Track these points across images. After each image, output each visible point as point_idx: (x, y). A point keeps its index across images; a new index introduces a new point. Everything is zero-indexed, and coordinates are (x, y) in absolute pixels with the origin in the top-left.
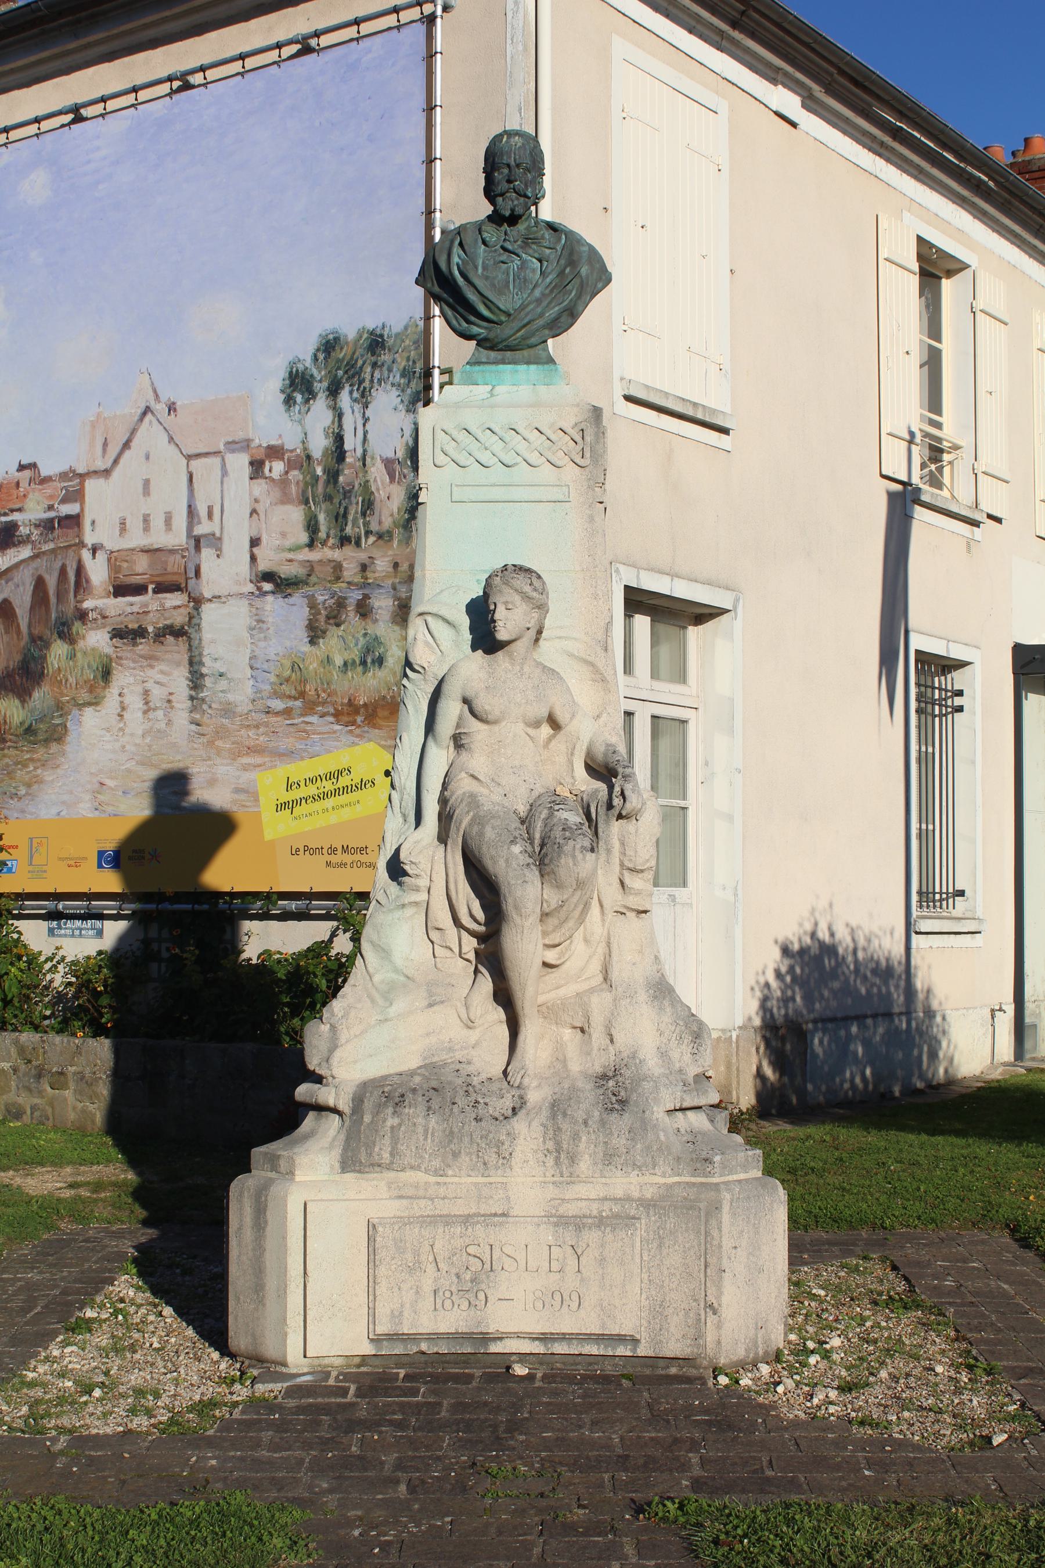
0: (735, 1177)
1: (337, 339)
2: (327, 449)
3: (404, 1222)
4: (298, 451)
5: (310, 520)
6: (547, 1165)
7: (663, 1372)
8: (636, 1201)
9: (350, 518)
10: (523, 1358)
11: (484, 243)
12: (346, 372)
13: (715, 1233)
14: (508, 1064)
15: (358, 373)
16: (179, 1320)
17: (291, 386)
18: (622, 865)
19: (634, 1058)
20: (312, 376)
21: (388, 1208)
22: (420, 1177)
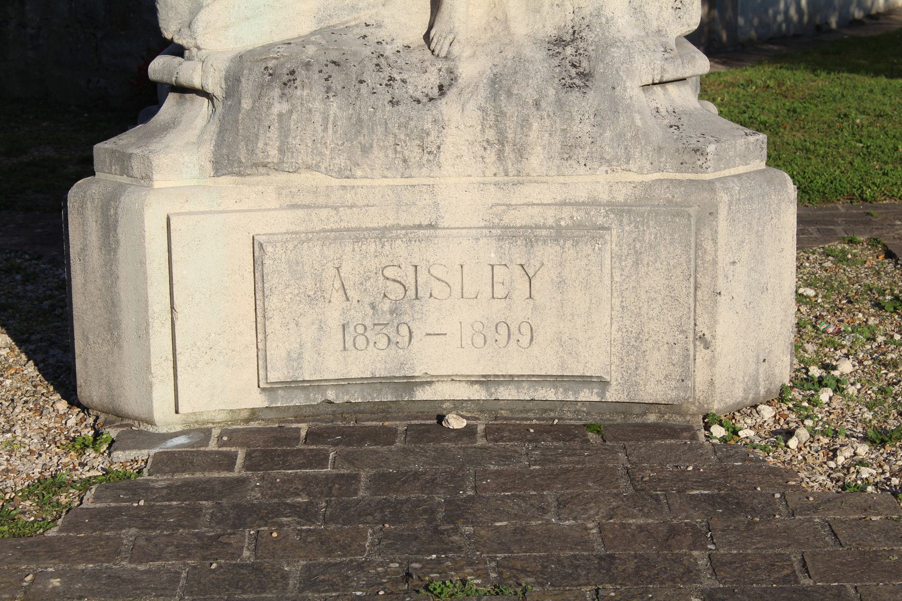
0: (733, 171)
3: (300, 238)
6: (487, 160)
7: (639, 420)
8: (604, 206)
10: (458, 405)
13: (708, 245)
14: (431, 27)
16: (17, 350)
19: (598, 15)
21: (278, 222)
22: (319, 179)
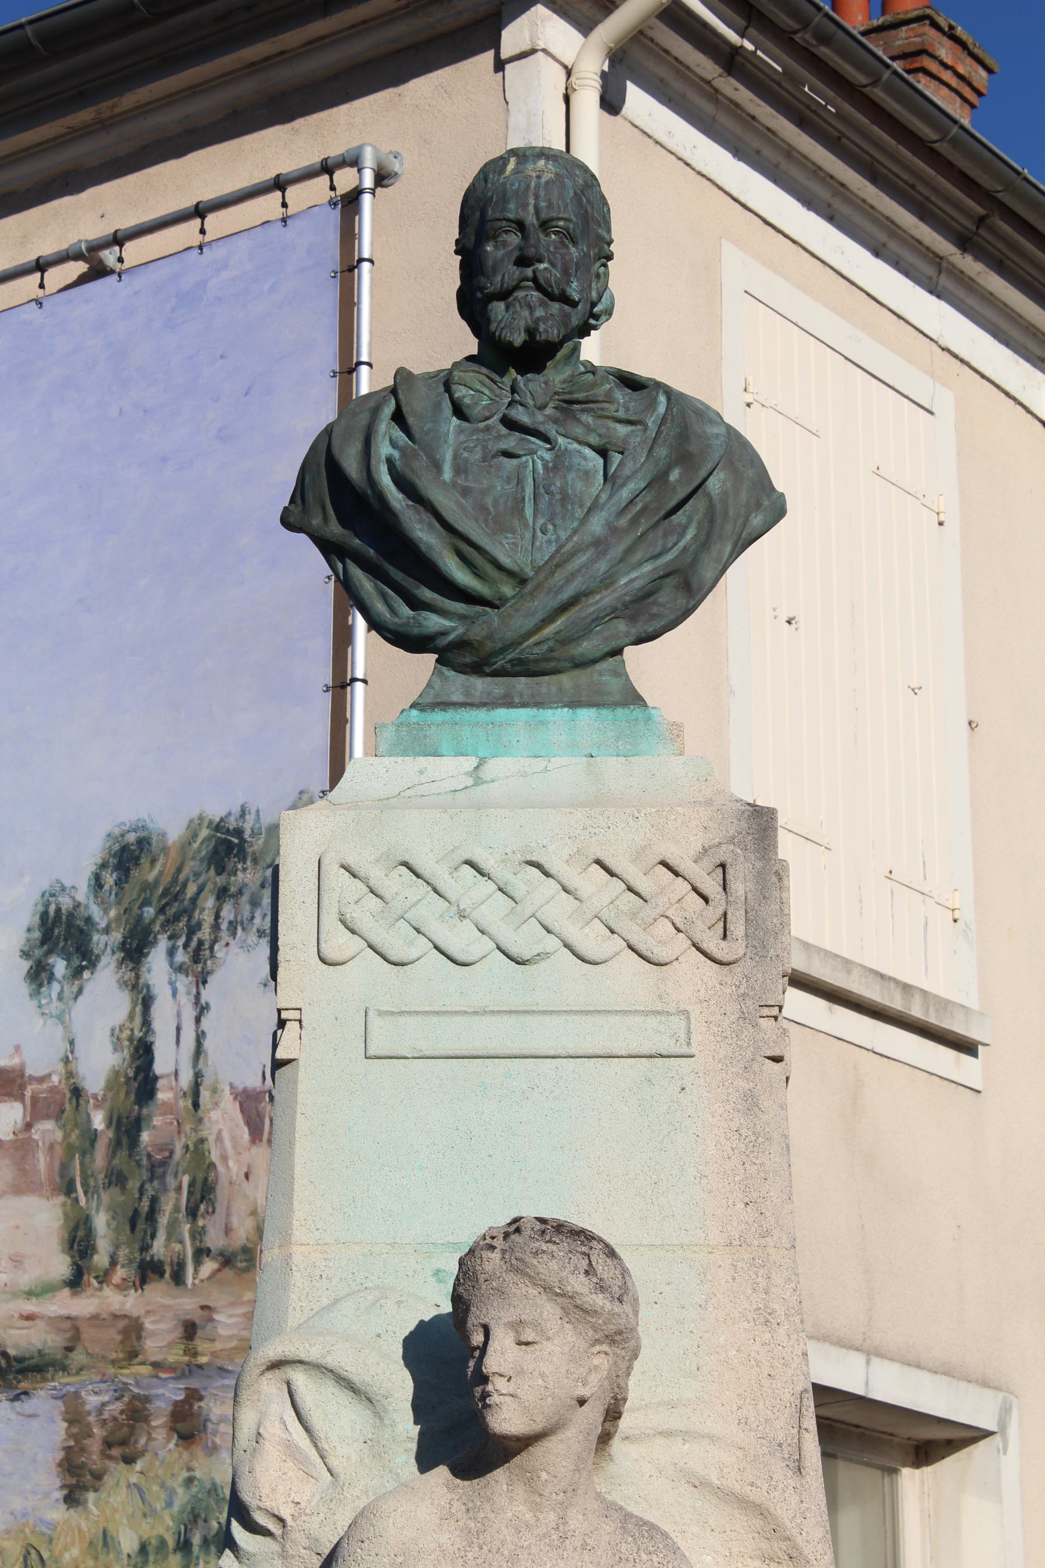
1: (143, 843)
2: (116, 1073)
4: (55, 1079)
5: (76, 1228)
9: (163, 1220)
11: (459, 411)
12: (161, 910)
15: (188, 912)
17: (43, 942)
20: (89, 920)
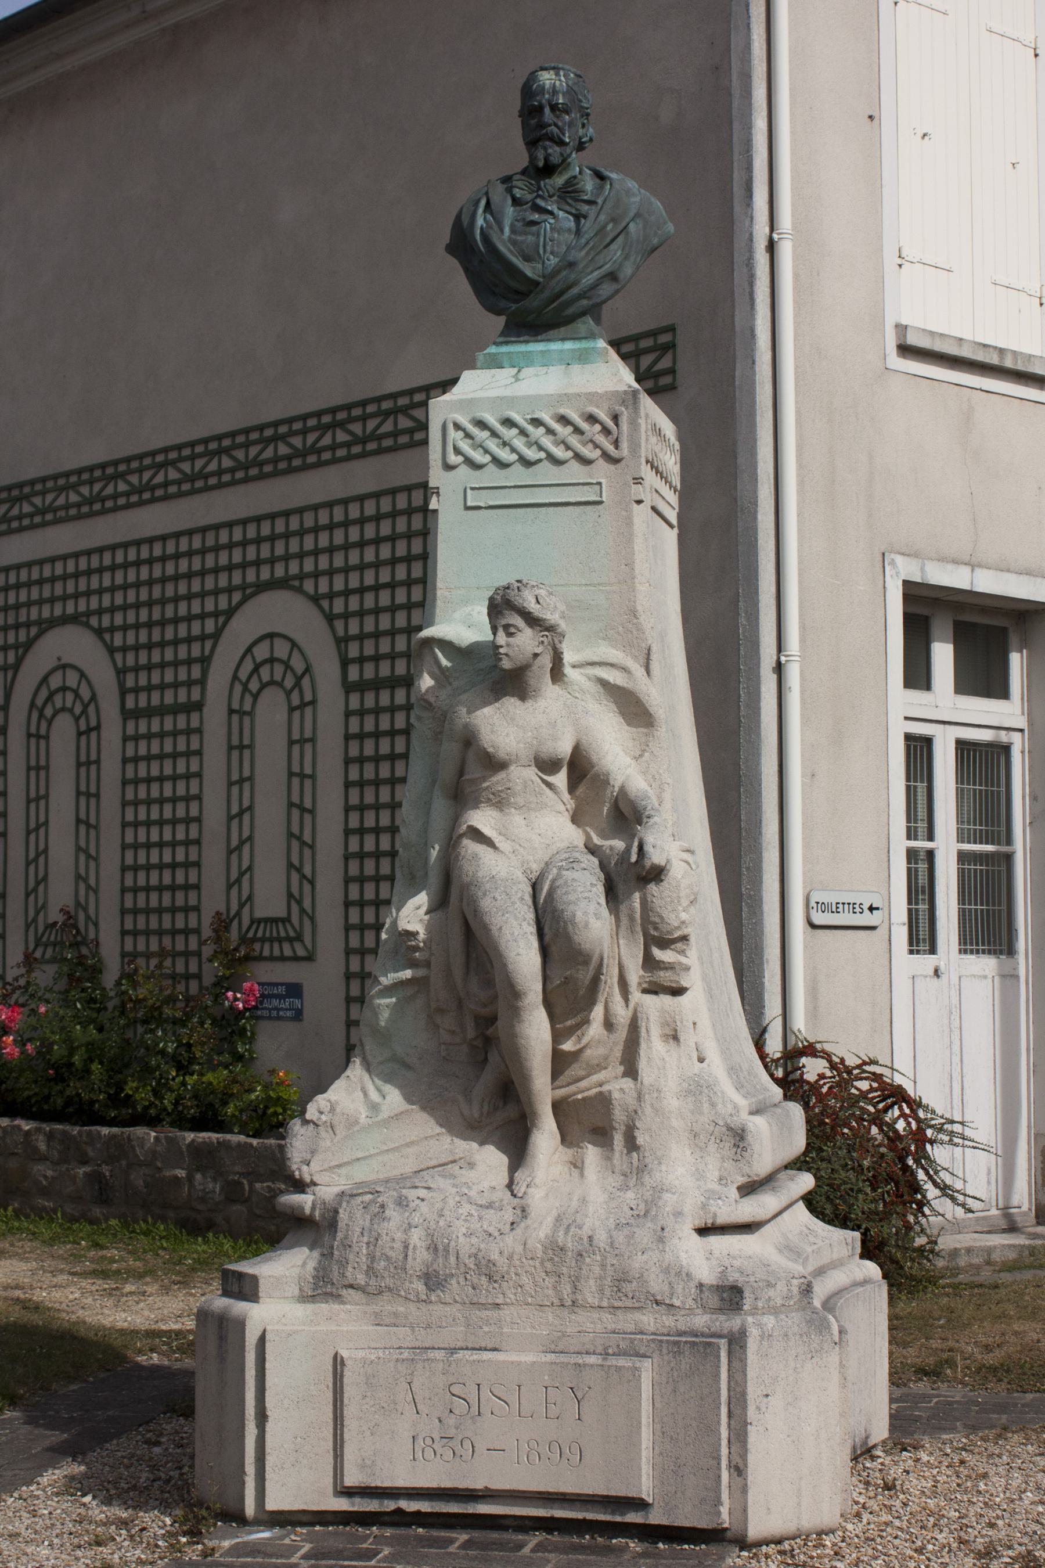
18: (646, 935)
